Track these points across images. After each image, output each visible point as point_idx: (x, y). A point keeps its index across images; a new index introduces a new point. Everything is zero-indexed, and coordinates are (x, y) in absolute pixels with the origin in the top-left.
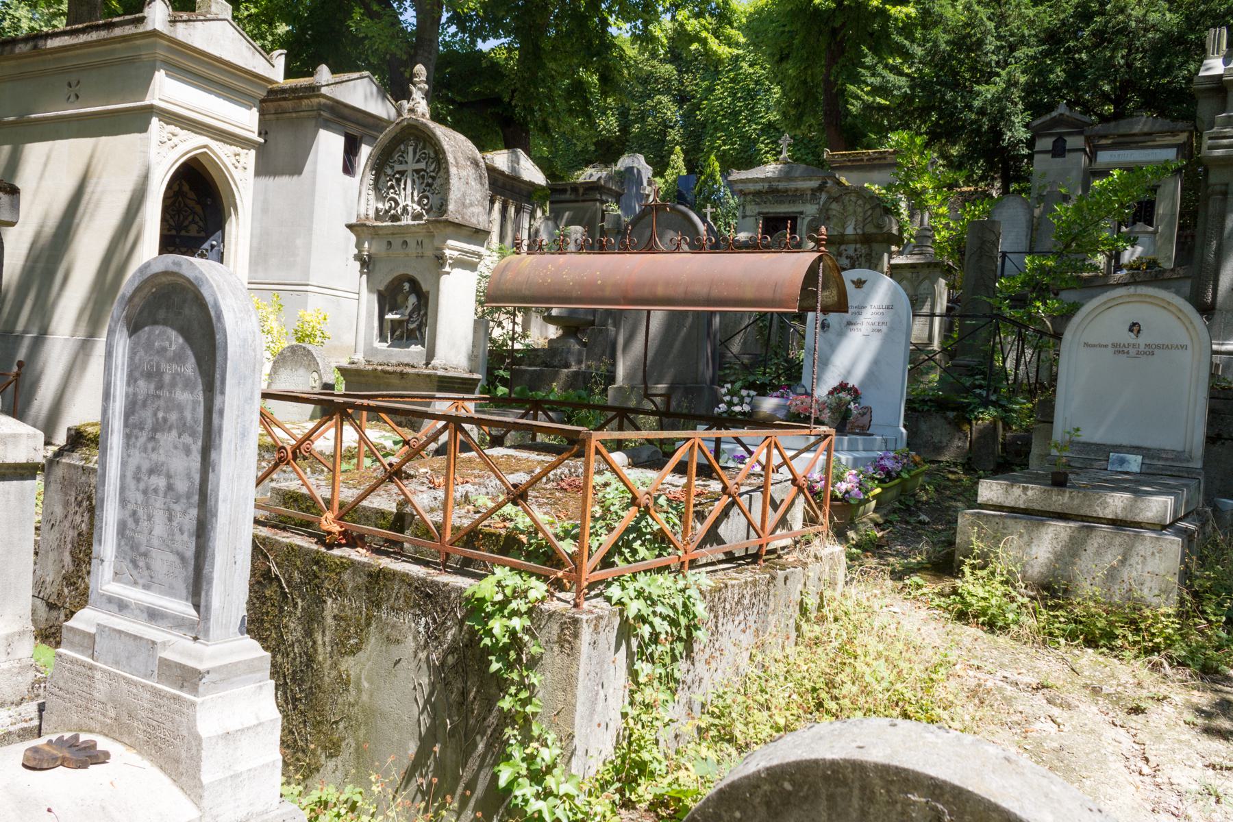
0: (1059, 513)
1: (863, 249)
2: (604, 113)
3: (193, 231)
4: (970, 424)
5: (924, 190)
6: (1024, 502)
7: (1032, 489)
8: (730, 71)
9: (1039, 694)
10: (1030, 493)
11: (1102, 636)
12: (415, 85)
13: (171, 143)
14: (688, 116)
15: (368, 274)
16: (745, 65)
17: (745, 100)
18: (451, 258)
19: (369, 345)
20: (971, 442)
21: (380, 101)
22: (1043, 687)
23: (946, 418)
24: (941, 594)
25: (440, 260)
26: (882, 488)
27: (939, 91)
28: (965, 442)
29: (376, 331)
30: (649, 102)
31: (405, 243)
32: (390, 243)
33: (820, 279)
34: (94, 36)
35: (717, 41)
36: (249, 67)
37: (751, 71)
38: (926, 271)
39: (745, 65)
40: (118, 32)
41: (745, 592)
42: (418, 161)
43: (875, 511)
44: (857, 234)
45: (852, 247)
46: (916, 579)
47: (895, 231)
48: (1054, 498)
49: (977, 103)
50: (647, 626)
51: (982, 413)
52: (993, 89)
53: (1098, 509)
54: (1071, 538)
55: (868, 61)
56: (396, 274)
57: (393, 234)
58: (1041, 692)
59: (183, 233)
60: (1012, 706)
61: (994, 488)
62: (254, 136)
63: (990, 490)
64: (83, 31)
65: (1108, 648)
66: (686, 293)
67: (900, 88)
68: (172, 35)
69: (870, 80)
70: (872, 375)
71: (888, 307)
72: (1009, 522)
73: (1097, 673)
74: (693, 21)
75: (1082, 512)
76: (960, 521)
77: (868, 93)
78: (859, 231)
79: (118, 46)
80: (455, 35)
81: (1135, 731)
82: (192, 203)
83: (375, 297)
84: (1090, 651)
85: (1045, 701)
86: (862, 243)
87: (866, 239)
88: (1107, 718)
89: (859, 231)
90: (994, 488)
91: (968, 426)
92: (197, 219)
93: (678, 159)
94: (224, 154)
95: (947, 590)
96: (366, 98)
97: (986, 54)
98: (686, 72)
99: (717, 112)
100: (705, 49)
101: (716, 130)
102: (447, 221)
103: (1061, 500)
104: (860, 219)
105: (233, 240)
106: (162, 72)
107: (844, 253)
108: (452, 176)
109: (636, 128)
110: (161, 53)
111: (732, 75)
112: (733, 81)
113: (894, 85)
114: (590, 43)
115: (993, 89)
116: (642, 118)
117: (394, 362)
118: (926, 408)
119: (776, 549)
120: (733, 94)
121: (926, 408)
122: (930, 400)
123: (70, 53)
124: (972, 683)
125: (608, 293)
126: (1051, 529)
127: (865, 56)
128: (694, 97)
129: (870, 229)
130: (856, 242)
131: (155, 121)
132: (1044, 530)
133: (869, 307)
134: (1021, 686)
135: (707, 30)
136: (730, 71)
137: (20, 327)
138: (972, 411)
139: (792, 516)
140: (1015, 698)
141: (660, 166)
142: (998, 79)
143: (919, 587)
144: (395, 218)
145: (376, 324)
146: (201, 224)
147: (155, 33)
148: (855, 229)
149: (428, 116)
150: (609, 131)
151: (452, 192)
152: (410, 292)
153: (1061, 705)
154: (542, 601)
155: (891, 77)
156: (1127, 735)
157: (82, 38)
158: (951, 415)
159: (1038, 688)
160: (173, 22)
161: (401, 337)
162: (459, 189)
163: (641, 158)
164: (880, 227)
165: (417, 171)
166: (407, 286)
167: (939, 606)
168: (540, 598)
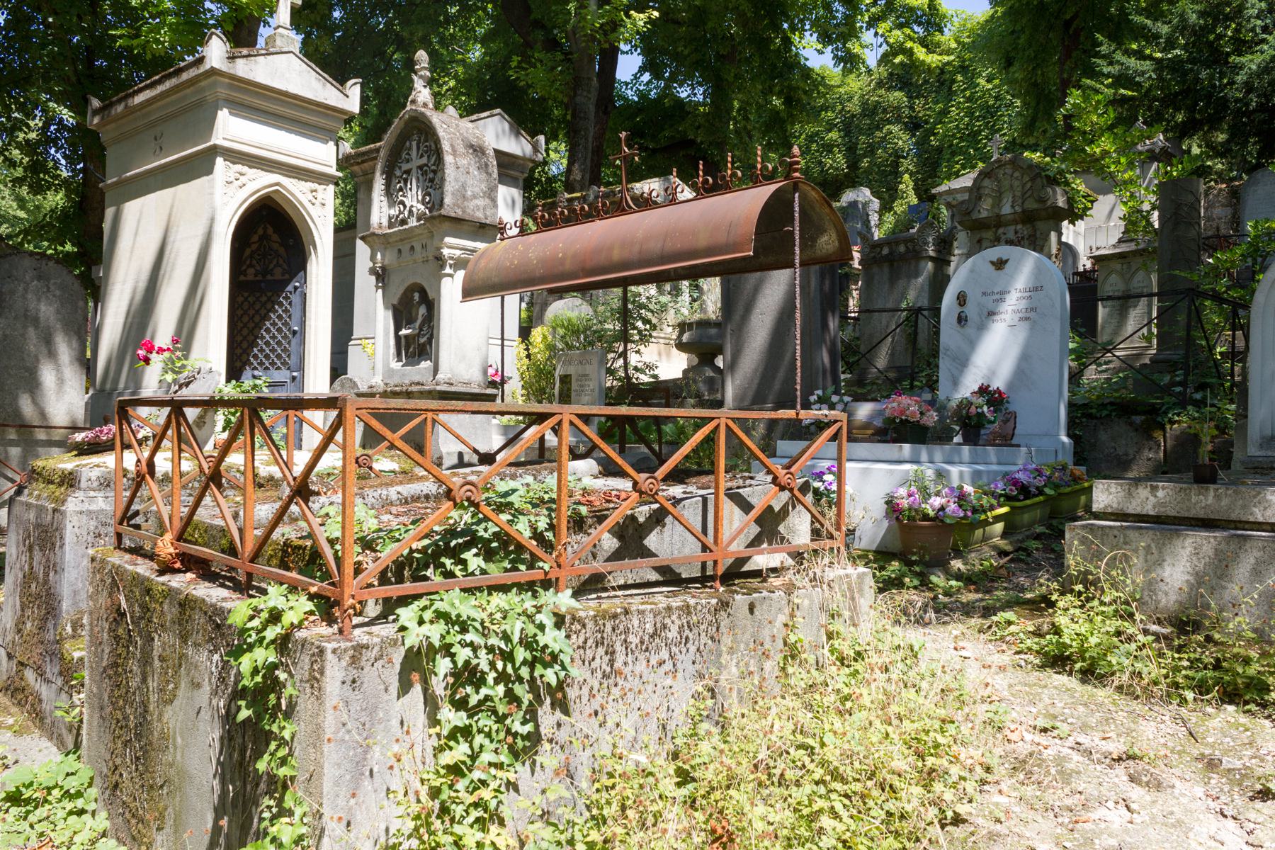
0: (1202, 520)
1: (1024, 230)
2: (831, 151)
3: (278, 274)
4: (1164, 429)
5: (1105, 153)
6: (1154, 507)
7: (1164, 488)
8: (965, 89)
9: (1120, 770)
10: (1160, 494)
11: (1248, 686)
12: (416, 73)
13: (239, 183)
14: (922, 144)
15: (384, 288)
16: (982, 81)
17: (984, 118)
18: (451, 258)
19: (386, 364)
20: (1165, 451)
21: (513, 139)
22: (1129, 757)
23: (1131, 424)
24: (1038, 633)
25: (440, 260)
26: (1012, 508)
27: (1192, 70)
28: (1157, 453)
29: (392, 350)
30: (878, 134)
31: (412, 248)
32: (400, 251)
33: (797, 215)
34: (168, 85)
35: (924, 50)
36: (340, 106)
37: (990, 86)
38: (1140, 260)
39: (982, 81)
40: (185, 76)
41: (667, 621)
42: (422, 156)
43: (1005, 535)
44: (1016, 213)
45: (1011, 229)
46: (1010, 615)
47: (1061, 202)
48: (1194, 499)
49: (1240, 78)
50: (448, 659)
51: (1178, 415)
52: (1258, 58)
53: (1256, 510)
54: (1217, 552)
55: (1104, 49)
56: (406, 284)
57: (401, 240)
58: (1123, 764)
59: (269, 277)
60: (1069, 784)
61: (1113, 490)
62: (333, 171)
63: (1105, 495)
64: (160, 82)
65: (1258, 705)
66: (640, 252)
67: (1143, 73)
68: (232, 71)
69: (1106, 70)
70: (1021, 373)
71: (1036, 289)
72: (1132, 535)
73: (1228, 740)
74: (897, 33)
75: (1233, 517)
76: (1067, 536)
77: (1108, 86)
78: (1018, 209)
79: (188, 91)
80: (650, 82)
81: (1252, 826)
82: (275, 246)
83: (390, 314)
84: (1231, 708)
85: (1126, 778)
86: (1024, 222)
87: (1028, 218)
88: (1212, 805)
89: (1018, 209)
90: (1113, 490)
91: (1161, 433)
92: (281, 261)
93: (907, 184)
94: (298, 191)
95: (1045, 627)
96: (497, 136)
97: (1249, 21)
98: (917, 97)
99: (954, 135)
100: (911, 60)
101: (953, 154)
102: (441, 216)
103: (1206, 500)
104: (1018, 194)
105: (314, 280)
106: (226, 111)
107: (1003, 237)
108: (447, 165)
109: (865, 163)
110: (222, 92)
111: (968, 93)
112: (969, 100)
113: (1135, 72)
114: (774, 66)
115: (1258, 58)
116: (871, 151)
117: (407, 382)
118: (1105, 413)
119: (761, 571)
120: (970, 113)
121: (1105, 413)
122: (1111, 404)
123: (154, 106)
124: (1023, 749)
125: (568, 266)
126: (1189, 541)
127: (1101, 44)
128: (927, 122)
129: (1031, 205)
130: (1015, 222)
131: (219, 161)
132: (1178, 542)
133: (1013, 292)
134: (1095, 756)
135: (911, 39)
136: (965, 89)
137: (121, 385)
138: (1166, 413)
139: (787, 528)
140: (1078, 773)
141: (888, 197)
142: (1265, 47)
143: (1009, 623)
144: (404, 222)
145: (392, 342)
146: (285, 266)
147: (213, 72)
148: (1013, 207)
149: (431, 106)
150: (837, 169)
151: (447, 184)
152: (420, 303)
153: (1147, 784)
154: (300, 626)
155: (1132, 62)
156: (1239, 831)
157: (160, 89)
158: (1138, 419)
159: (1120, 759)
160: (232, 58)
161: (413, 356)
162: (456, 180)
163: (867, 191)
164: (1042, 200)
165: (420, 167)
166: (416, 296)
167: (1030, 649)
168: (296, 622)
